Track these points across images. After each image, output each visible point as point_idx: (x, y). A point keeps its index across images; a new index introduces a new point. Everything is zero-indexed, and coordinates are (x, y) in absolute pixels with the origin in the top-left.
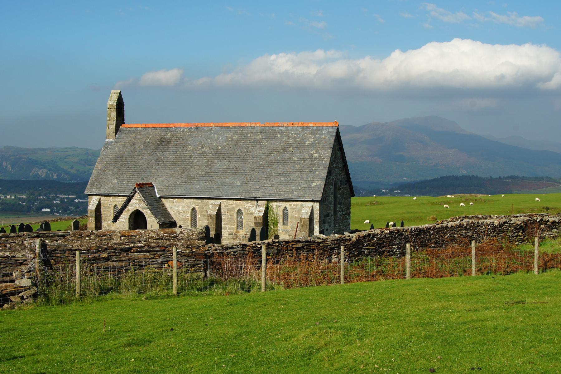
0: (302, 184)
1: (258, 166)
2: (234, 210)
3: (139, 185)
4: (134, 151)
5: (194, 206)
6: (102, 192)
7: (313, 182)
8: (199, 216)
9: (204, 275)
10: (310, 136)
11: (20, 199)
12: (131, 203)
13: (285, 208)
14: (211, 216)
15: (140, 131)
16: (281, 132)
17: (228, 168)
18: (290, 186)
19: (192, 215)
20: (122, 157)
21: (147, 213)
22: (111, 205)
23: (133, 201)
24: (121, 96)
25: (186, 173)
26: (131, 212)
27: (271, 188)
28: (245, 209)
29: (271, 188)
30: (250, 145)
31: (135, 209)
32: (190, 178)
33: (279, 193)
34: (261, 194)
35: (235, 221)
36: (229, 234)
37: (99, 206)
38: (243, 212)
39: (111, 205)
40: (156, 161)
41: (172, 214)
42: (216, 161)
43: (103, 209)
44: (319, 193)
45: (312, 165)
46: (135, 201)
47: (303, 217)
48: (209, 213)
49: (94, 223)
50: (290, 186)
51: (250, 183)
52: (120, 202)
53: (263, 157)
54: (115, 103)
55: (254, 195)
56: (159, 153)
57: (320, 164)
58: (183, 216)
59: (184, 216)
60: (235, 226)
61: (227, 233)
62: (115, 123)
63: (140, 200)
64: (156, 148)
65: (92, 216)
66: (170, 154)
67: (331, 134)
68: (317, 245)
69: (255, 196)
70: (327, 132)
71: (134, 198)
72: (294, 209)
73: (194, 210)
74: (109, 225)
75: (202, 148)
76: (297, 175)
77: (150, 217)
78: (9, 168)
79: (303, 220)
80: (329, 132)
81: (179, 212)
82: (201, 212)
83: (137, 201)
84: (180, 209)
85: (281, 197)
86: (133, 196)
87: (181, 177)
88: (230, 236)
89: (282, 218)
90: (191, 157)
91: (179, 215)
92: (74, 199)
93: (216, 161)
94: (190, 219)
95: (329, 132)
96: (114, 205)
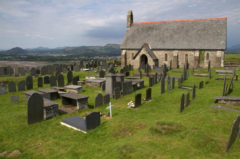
0: (215, 43)
1: (193, 36)
2: (184, 54)
3: (144, 44)
4: (139, 32)
5: (166, 53)
6: (128, 47)
7: (220, 42)
8: (168, 56)
9: (140, 48)
10: (215, 24)
11: (86, 58)
12: (141, 51)
13: (208, 53)
14: (175, 56)
15: (140, 25)
16: (201, 23)
17: (180, 37)
18: (210, 44)
19: (165, 56)
20: (134, 35)
21: (148, 55)
22: (131, 53)
23: (142, 51)
24: (132, 14)
25: (162, 40)
26: (141, 55)
27: (201, 45)
28: (189, 54)
29: (201, 45)
30: (188, 28)
31: (143, 54)
32: (164, 42)
33: (205, 46)
34: (197, 47)
35: (185, 59)
36: (182, 64)
37: (126, 53)
38: (188, 55)
39: (131, 53)
40: (148, 36)
41: (157, 56)
42: (174, 35)
43: (127, 54)
44: (224, 47)
45: (218, 35)
46: (142, 51)
47: (218, 57)
48: (174, 55)
49: (124, 60)
50: (210, 44)
51: (191, 43)
52: (135, 52)
53: (195, 32)
54: (130, 15)
55: (194, 48)
56: (149, 33)
57: (222, 35)
58: (161, 57)
59: (162, 57)
60: (185, 60)
61: (181, 64)
62: (130, 22)
63: (144, 50)
64: (148, 31)
65: (123, 57)
66: (155, 32)
67: (225, 22)
68: (114, 68)
69: (194, 48)
70: (222, 22)
71: (142, 49)
72: (212, 53)
73: (166, 54)
74: (130, 61)
75: (167, 30)
76: (212, 39)
77: (149, 57)
78: (84, 51)
79: (218, 58)
80: (223, 22)
81: (160, 55)
82: (169, 55)
83: (144, 51)
84: (160, 54)
85: (206, 48)
86: (142, 49)
87: (160, 41)
88: (182, 65)
89: (206, 57)
90: (163, 33)
91: (160, 57)
92: (98, 58)
93: (174, 35)
94: (164, 58)
95: (223, 22)
96: (132, 53)
